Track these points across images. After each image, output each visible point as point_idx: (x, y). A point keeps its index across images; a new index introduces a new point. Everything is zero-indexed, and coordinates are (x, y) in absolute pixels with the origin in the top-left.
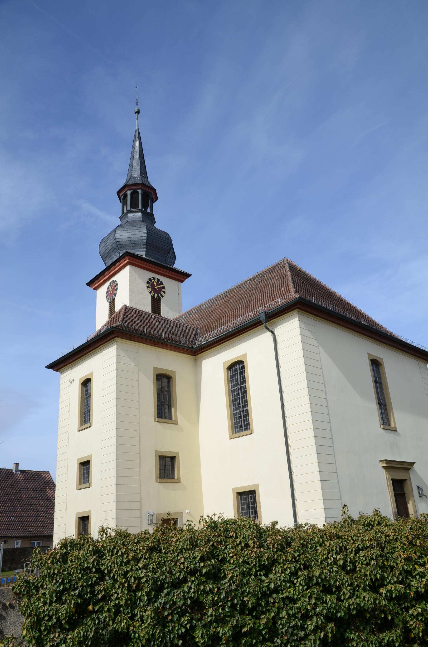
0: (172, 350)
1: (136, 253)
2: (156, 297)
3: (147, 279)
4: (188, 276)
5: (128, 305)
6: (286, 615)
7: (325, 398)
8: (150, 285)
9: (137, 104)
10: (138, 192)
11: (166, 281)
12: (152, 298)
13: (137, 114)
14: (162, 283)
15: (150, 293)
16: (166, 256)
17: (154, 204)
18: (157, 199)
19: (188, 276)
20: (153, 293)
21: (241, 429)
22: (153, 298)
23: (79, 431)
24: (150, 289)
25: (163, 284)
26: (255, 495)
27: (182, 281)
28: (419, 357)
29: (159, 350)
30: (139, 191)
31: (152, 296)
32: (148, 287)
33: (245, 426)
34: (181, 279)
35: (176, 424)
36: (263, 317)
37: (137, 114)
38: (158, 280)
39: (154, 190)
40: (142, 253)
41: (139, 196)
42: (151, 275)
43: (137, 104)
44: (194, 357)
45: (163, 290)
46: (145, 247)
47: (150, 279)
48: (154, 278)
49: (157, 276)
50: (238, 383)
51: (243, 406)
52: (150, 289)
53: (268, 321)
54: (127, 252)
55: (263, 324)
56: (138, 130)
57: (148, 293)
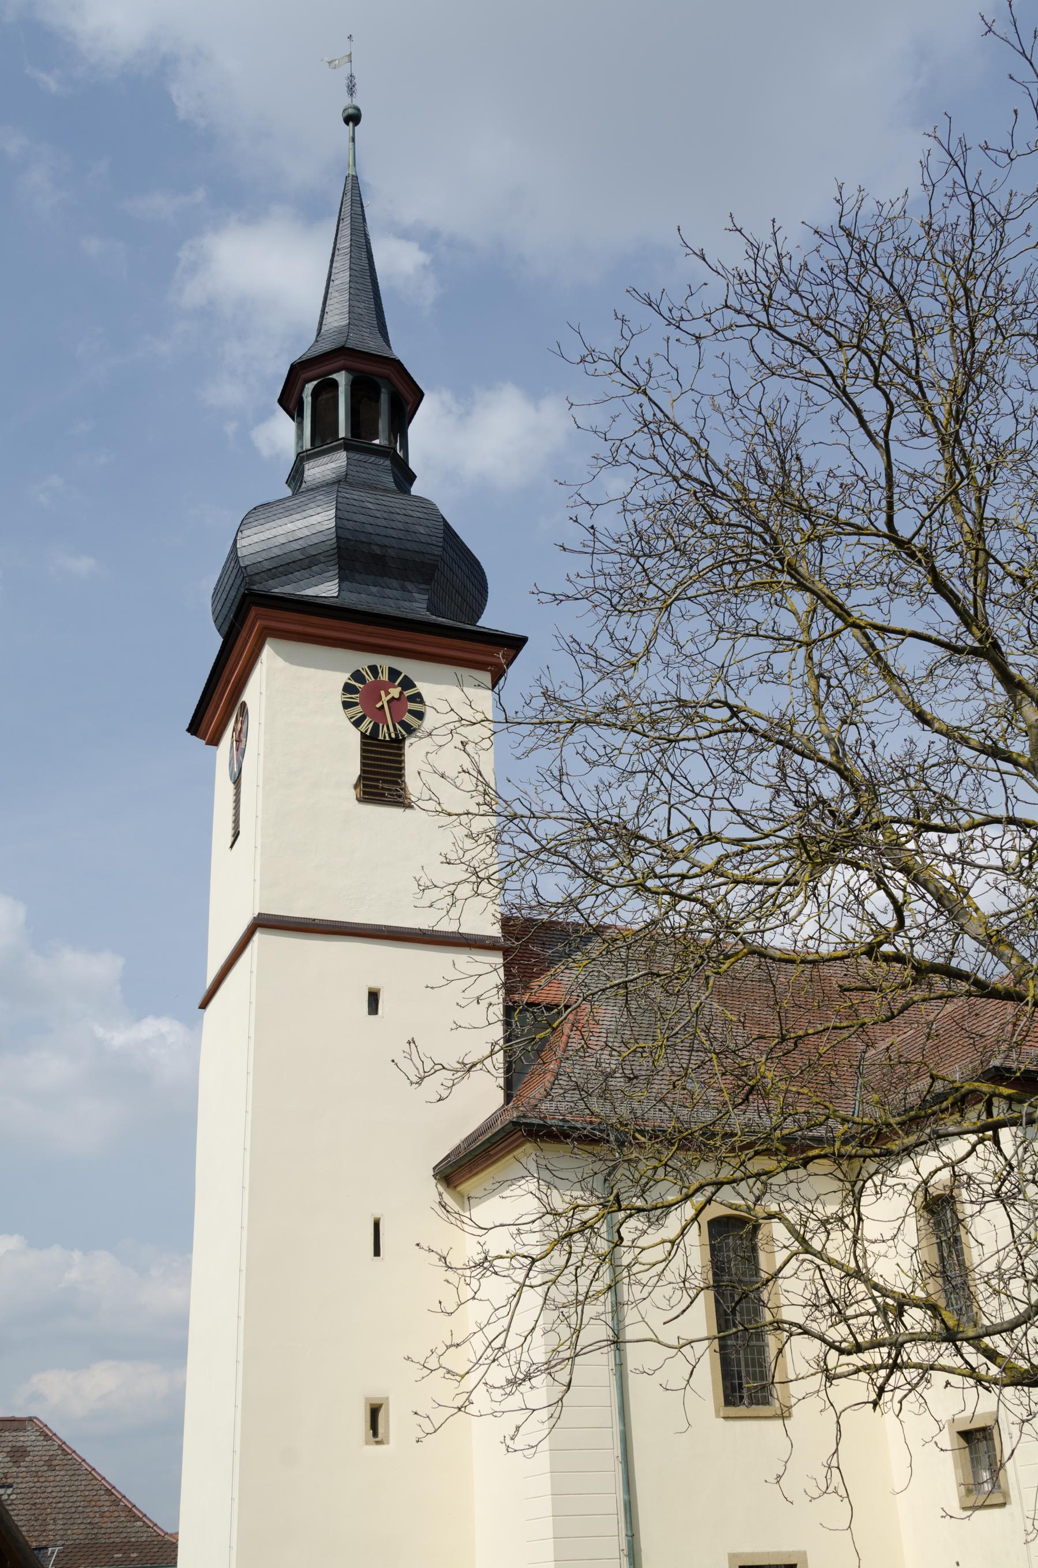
1: (310, 592)
6: (811, 1239)
7: (674, 832)
9: (351, 89)
10: (335, 384)
12: (363, 744)
13: (351, 124)
14: (408, 684)
15: (357, 723)
20: (367, 725)
25: (400, 673)
26: (761, 1343)
30: (342, 378)
31: (363, 735)
32: (347, 705)
37: (351, 124)
38: (394, 673)
40: (327, 589)
42: (362, 661)
43: (351, 89)
45: (411, 706)
48: (374, 669)
49: (385, 662)
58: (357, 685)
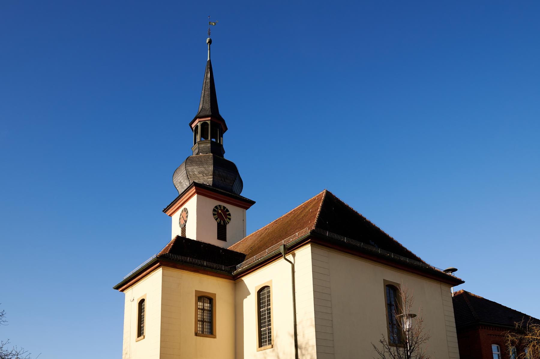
0: (213, 276)
2: (221, 224)
3: (213, 207)
4: (253, 203)
5: (180, 235)
8: (216, 213)
11: (230, 208)
14: (227, 211)
15: (216, 220)
16: (232, 185)
17: (224, 135)
18: (226, 129)
19: (253, 203)
20: (219, 220)
21: (266, 343)
22: (219, 224)
23: (136, 342)
24: (217, 216)
27: (247, 208)
28: (441, 281)
29: (201, 276)
31: (218, 223)
32: (214, 215)
33: (269, 341)
34: (246, 206)
35: (214, 338)
36: (282, 250)
39: (223, 121)
41: (208, 127)
42: (217, 203)
44: (234, 281)
46: (212, 177)
47: (216, 207)
50: (266, 305)
51: (268, 324)
52: (217, 216)
53: (287, 253)
54: (194, 182)
55: (282, 256)
56: (209, 62)
57: (214, 220)
58: (216, 210)
